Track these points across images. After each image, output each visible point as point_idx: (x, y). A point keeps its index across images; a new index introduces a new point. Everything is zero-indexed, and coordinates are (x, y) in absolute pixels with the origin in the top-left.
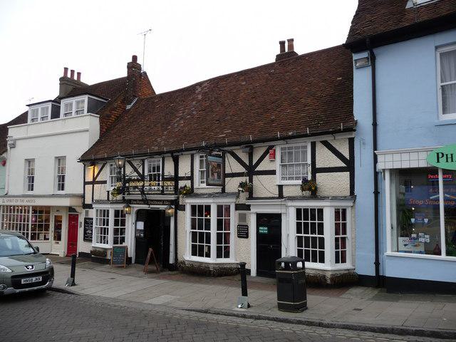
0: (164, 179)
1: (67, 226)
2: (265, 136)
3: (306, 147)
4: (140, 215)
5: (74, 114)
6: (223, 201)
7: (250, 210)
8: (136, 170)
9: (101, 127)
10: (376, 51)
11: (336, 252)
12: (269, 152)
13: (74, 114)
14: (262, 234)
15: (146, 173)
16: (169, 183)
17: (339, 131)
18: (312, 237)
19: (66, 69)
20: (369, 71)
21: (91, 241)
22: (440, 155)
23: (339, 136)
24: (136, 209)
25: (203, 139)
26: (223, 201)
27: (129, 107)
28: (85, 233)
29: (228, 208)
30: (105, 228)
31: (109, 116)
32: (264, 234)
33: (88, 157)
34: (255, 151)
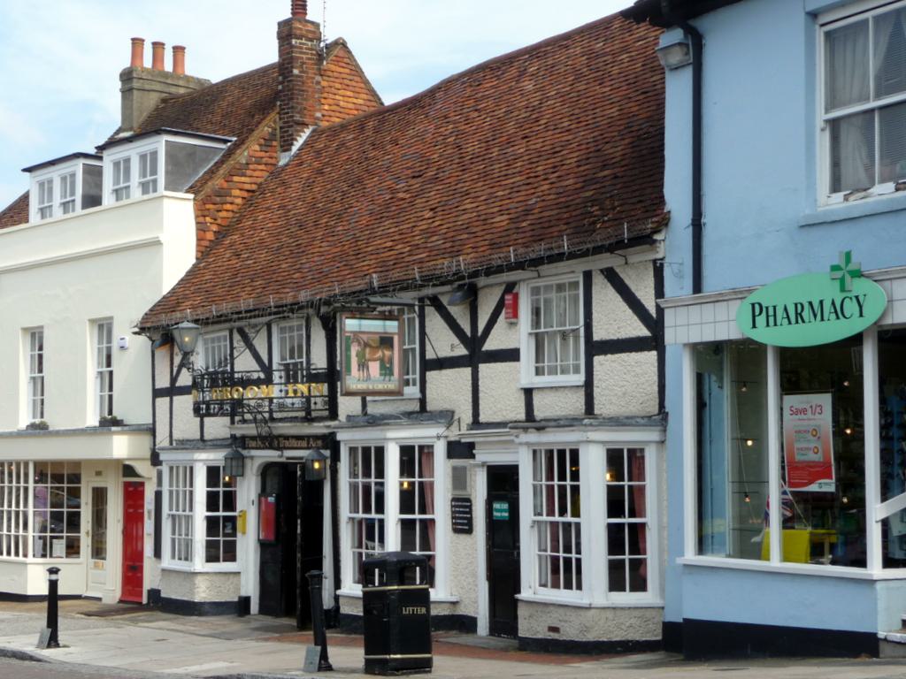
6: (416, 434)
7: (473, 456)
10: (706, 24)
12: (507, 305)
19: (137, 43)
20: (687, 76)
22: (757, 307)
24: (257, 463)
26: (416, 434)
29: (426, 451)
30: (567, 526)
31: (222, 194)
34: (481, 295)
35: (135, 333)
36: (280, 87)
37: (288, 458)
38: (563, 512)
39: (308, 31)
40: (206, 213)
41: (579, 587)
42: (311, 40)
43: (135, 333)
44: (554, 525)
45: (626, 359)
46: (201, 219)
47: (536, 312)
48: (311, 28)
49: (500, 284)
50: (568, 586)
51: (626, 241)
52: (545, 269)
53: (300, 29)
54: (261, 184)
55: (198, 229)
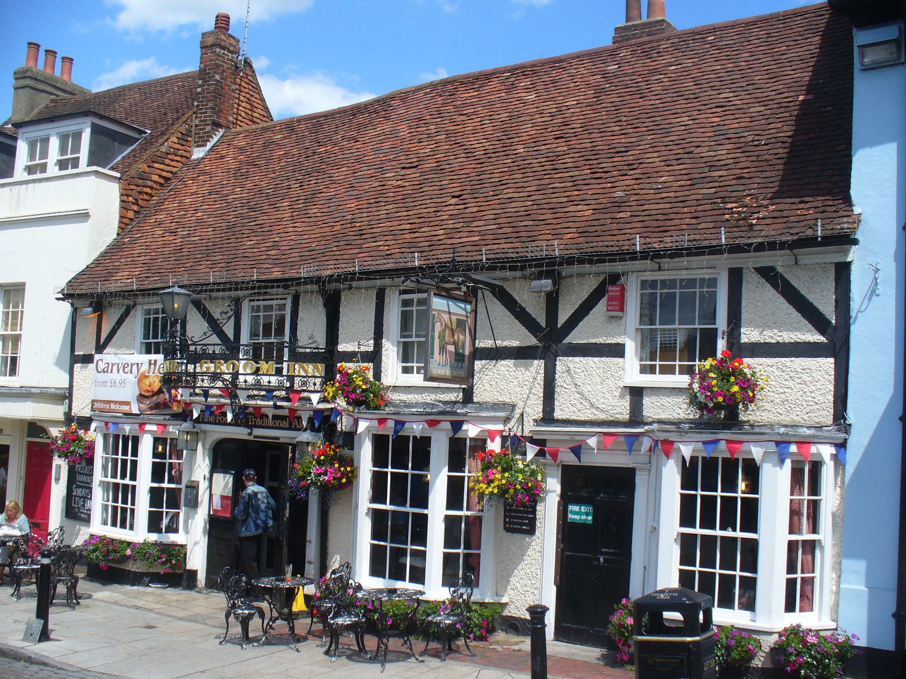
0: (297, 357)
1: (23, 474)
2: (599, 245)
3: (713, 282)
4: (225, 457)
5: (53, 170)
8: (215, 327)
9: (124, 206)
11: (788, 580)
13: (53, 170)
14: (574, 524)
15: (245, 338)
16: (310, 368)
17: (810, 242)
18: (723, 538)
21: (87, 521)
23: (809, 257)
25: (412, 246)
27: (198, 153)
28: (69, 499)
30: (126, 487)
31: (143, 176)
32: (582, 526)
33: (85, 289)
35: (58, 299)
36: (199, 90)
37: (255, 437)
38: (123, 477)
39: (230, 44)
40: (130, 192)
41: (132, 528)
42: (232, 52)
43: (58, 299)
44: (116, 486)
45: (788, 364)
46: (125, 198)
47: (406, 319)
48: (232, 41)
49: (598, 274)
50: (123, 526)
51: (819, 239)
52: (666, 262)
53: (225, 41)
54: (176, 173)
55: (122, 207)
